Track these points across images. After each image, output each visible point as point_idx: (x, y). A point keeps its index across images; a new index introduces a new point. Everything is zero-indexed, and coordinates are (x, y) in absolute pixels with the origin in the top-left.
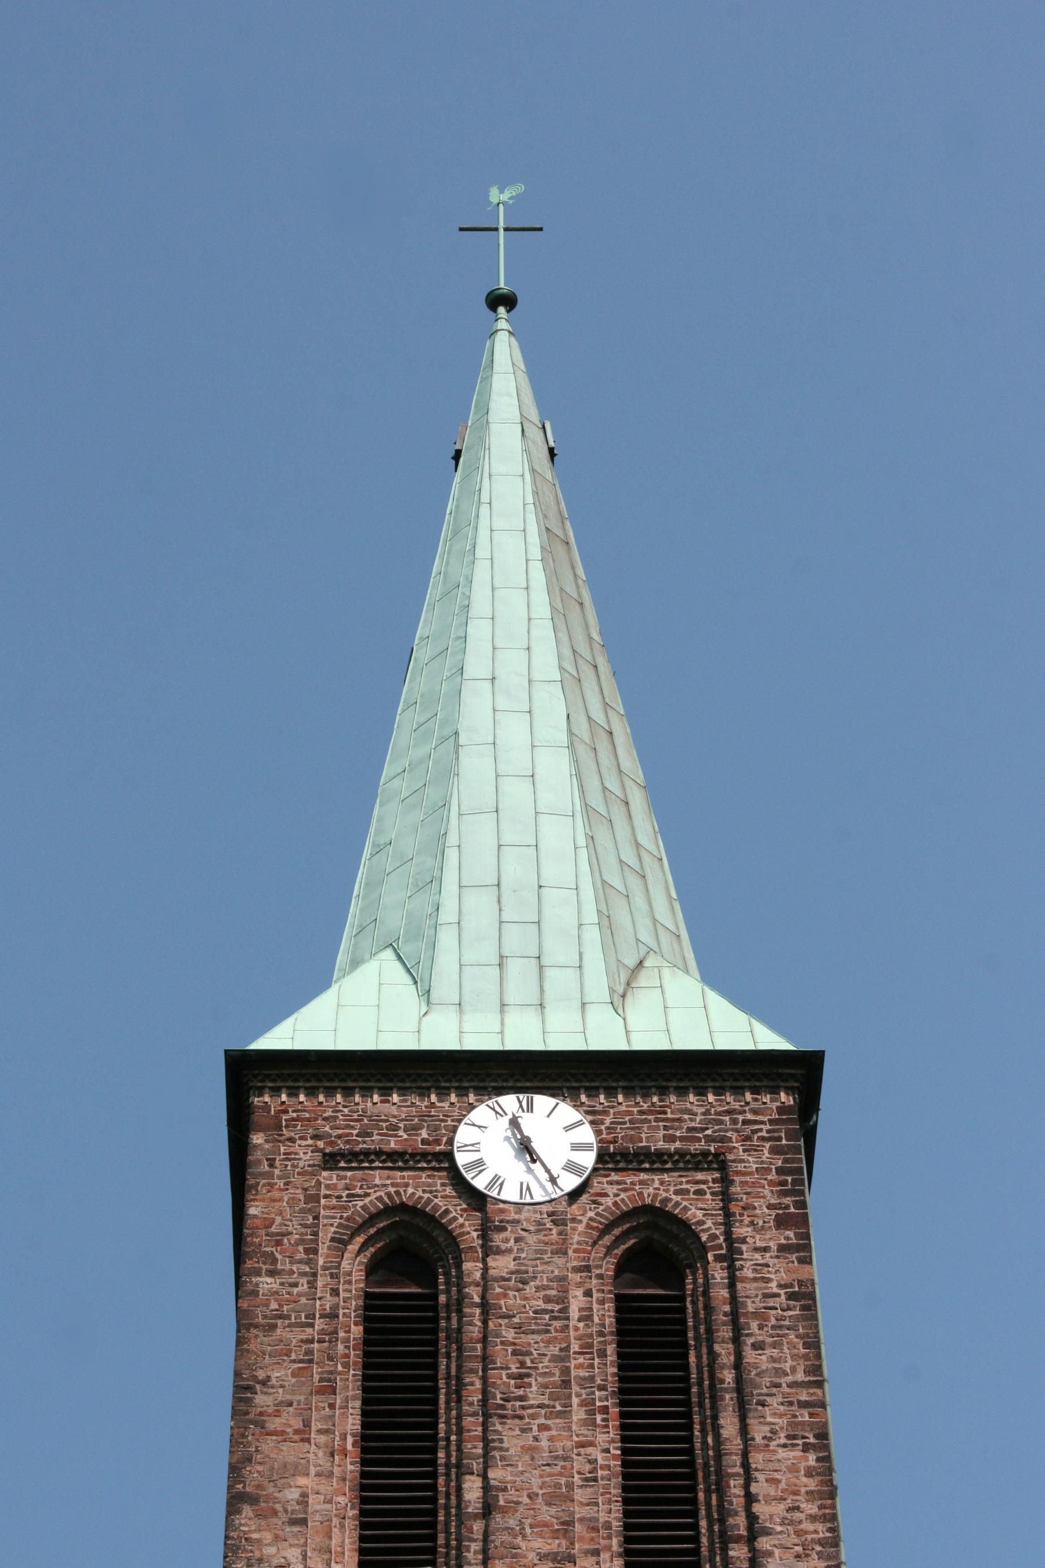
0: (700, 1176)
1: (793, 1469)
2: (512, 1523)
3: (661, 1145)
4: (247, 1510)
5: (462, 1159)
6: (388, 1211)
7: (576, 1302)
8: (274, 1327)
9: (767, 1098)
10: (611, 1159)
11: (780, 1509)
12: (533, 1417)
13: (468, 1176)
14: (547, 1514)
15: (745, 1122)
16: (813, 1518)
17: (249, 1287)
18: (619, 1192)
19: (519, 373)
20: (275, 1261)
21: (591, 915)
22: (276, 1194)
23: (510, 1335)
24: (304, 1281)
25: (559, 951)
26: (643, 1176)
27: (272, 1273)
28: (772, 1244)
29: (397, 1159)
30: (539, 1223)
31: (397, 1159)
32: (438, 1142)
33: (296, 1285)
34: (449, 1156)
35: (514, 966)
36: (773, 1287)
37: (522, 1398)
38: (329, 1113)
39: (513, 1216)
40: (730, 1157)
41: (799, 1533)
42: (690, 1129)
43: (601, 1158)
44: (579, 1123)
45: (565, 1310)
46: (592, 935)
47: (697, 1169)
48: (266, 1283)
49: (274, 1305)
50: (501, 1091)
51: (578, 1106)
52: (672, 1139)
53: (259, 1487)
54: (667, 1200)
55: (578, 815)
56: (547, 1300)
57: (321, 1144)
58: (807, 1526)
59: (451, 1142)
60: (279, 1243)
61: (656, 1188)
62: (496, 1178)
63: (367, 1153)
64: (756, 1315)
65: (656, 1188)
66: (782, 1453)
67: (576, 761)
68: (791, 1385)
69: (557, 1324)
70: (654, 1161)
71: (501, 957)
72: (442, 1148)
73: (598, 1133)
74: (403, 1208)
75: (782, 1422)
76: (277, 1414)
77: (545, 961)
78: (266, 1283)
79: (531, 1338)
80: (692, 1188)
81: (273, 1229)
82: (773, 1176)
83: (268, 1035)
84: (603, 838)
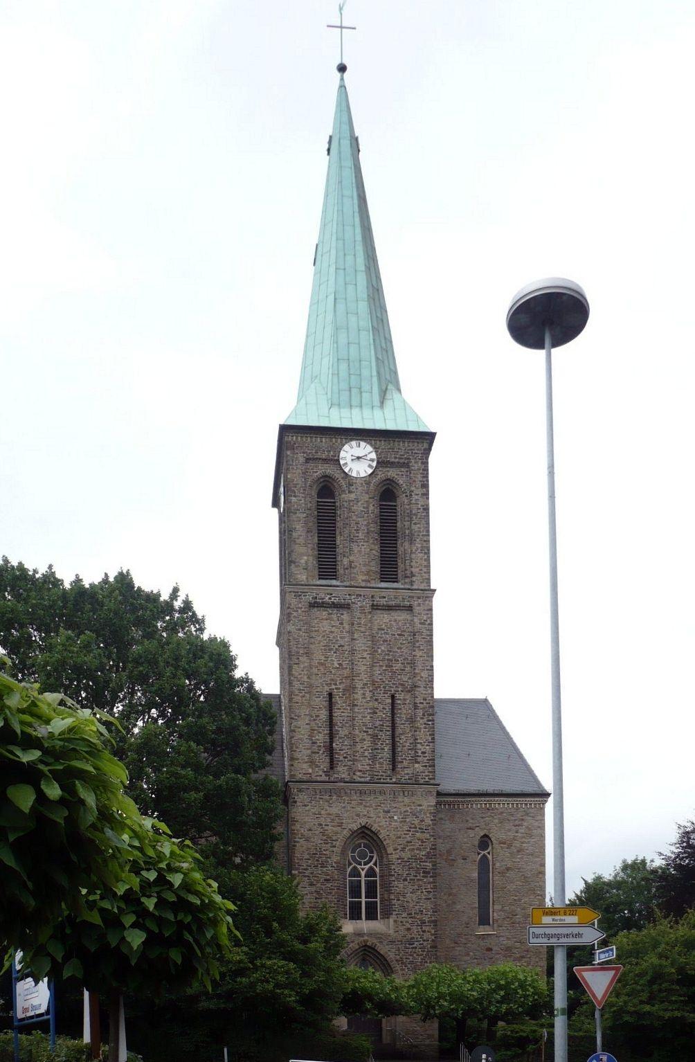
0: (402, 469)
1: (421, 559)
2: (355, 571)
3: (393, 460)
4: (293, 565)
5: (342, 462)
6: (323, 477)
7: (371, 508)
8: (296, 513)
9: (420, 446)
10: (381, 463)
11: (417, 570)
12: (361, 542)
13: (343, 468)
14: (364, 569)
15: (415, 453)
16: (425, 573)
17: (289, 501)
18: (381, 476)
19: (347, 202)
20: (295, 493)
21: (375, 373)
22: (294, 471)
23: (354, 518)
24: (303, 499)
25: (366, 387)
26: (388, 469)
27: (295, 496)
28: (420, 493)
29: (326, 461)
30: (362, 484)
31: (326, 461)
32: (335, 456)
33: (301, 500)
34: (338, 460)
35: (345, 200)
36: (419, 506)
37: (358, 537)
38: (307, 445)
39: (355, 481)
40: (411, 464)
41: (422, 576)
42: (401, 455)
43: (378, 463)
44: (371, 452)
45: (368, 511)
46: (375, 379)
47: (401, 467)
48: (294, 499)
49: (296, 506)
50: (351, 440)
51: (371, 445)
52: (396, 458)
53: (296, 559)
54: (393, 477)
55: (371, 330)
56: (364, 508)
57: (305, 455)
58: (424, 574)
59: (339, 457)
60: (296, 487)
61: (392, 473)
62: (351, 469)
63: (317, 458)
64: (414, 514)
65: (392, 473)
66: (419, 555)
67: (370, 304)
68: (422, 535)
69: (366, 515)
70: (392, 465)
71: (350, 391)
72: (335, 458)
73: (377, 455)
74: (326, 476)
75: (419, 546)
76: (298, 538)
77: (362, 390)
78: (294, 499)
79: (360, 519)
80: (400, 473)
81: (294, 483)
82: (421, 471)
83: (552, 805)
84: (378, 341)
